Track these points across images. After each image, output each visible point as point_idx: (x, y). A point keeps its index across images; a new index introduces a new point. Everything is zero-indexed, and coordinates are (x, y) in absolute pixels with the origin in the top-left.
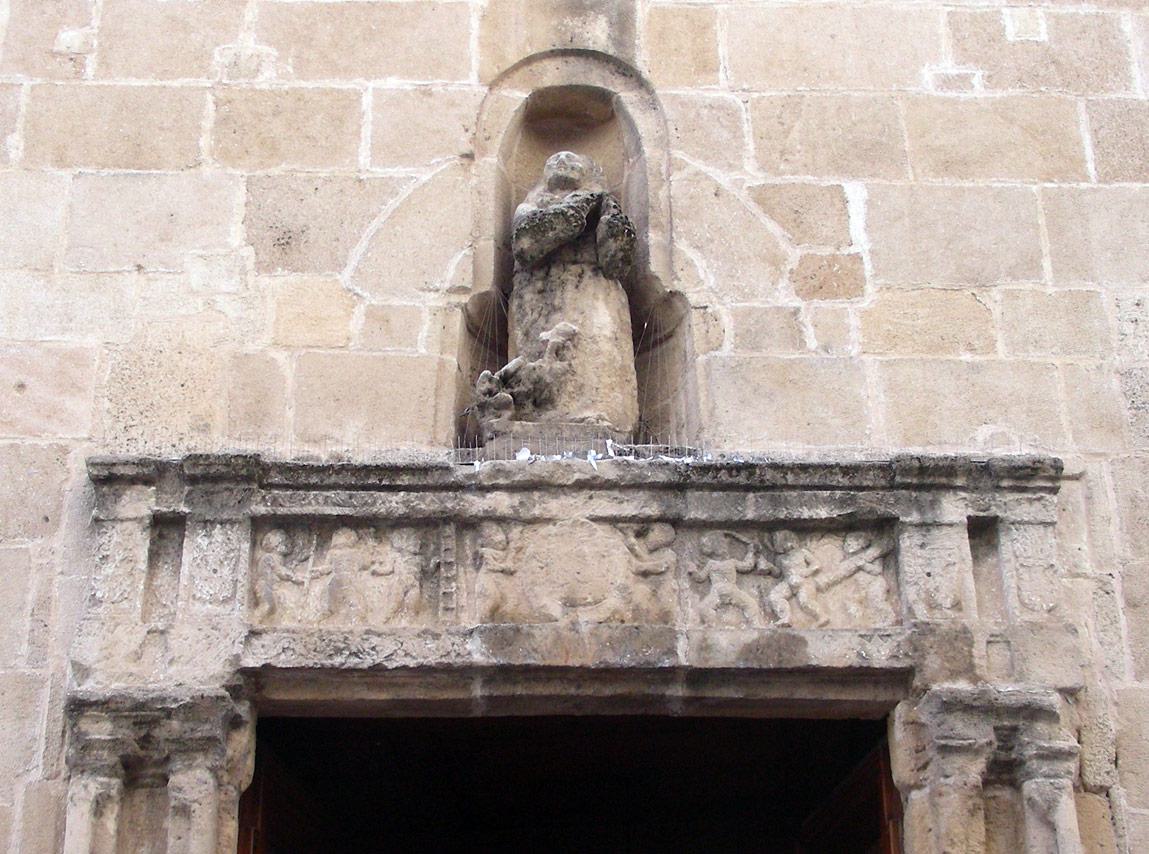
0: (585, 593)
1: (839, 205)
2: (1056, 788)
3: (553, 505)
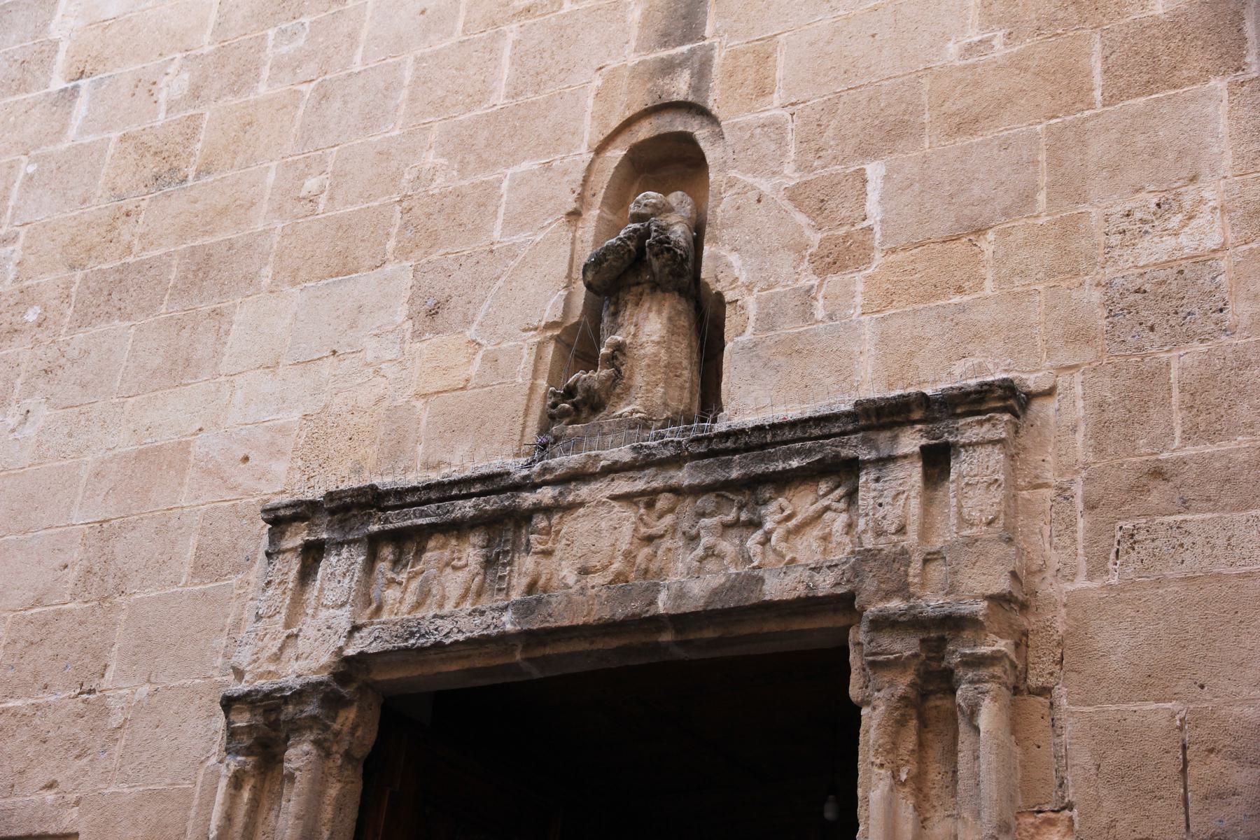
0: (594, 562)
1: (859, 185)
2: (980, 693)
3: (584, 491)
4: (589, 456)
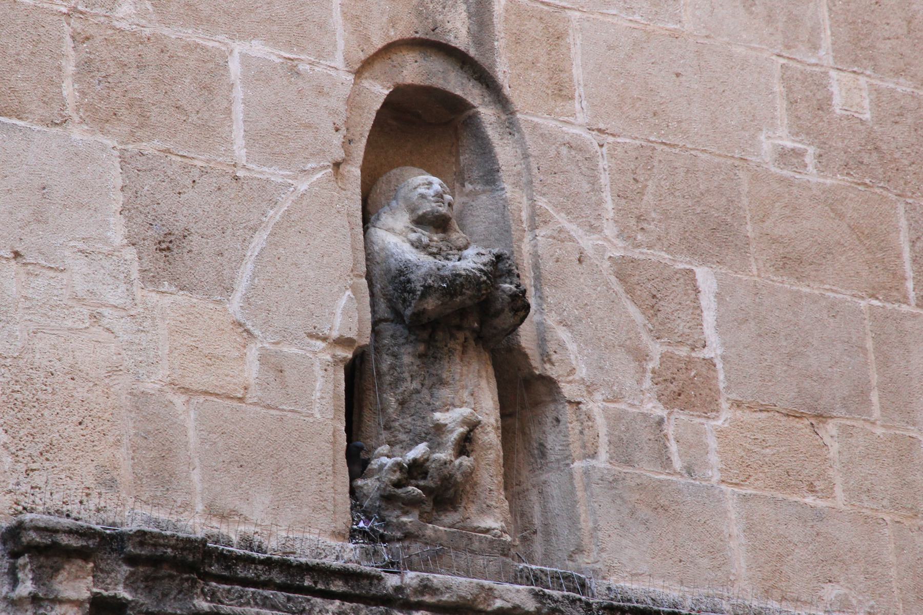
4: (482, 587)
